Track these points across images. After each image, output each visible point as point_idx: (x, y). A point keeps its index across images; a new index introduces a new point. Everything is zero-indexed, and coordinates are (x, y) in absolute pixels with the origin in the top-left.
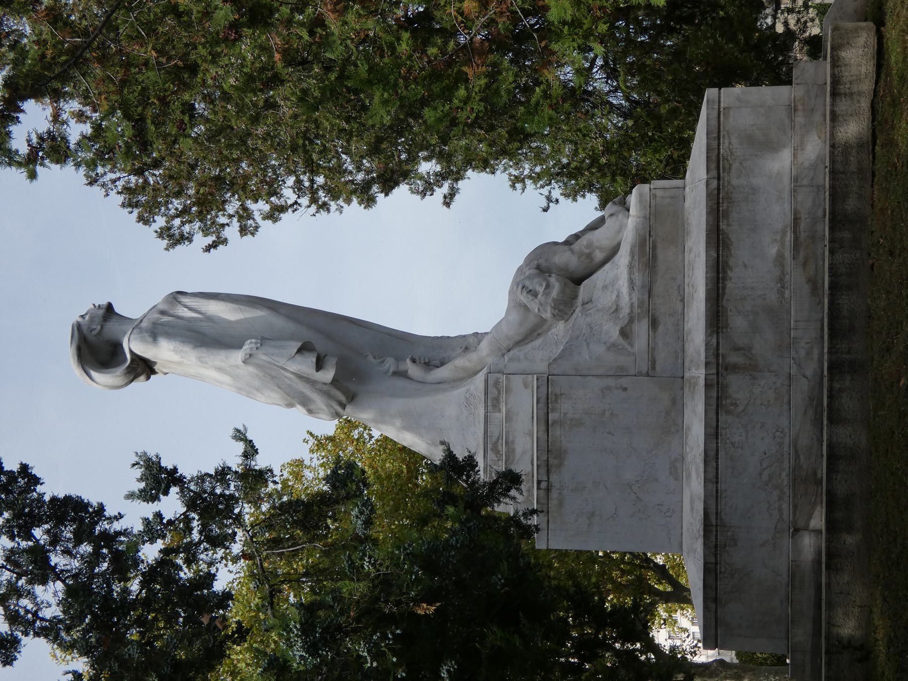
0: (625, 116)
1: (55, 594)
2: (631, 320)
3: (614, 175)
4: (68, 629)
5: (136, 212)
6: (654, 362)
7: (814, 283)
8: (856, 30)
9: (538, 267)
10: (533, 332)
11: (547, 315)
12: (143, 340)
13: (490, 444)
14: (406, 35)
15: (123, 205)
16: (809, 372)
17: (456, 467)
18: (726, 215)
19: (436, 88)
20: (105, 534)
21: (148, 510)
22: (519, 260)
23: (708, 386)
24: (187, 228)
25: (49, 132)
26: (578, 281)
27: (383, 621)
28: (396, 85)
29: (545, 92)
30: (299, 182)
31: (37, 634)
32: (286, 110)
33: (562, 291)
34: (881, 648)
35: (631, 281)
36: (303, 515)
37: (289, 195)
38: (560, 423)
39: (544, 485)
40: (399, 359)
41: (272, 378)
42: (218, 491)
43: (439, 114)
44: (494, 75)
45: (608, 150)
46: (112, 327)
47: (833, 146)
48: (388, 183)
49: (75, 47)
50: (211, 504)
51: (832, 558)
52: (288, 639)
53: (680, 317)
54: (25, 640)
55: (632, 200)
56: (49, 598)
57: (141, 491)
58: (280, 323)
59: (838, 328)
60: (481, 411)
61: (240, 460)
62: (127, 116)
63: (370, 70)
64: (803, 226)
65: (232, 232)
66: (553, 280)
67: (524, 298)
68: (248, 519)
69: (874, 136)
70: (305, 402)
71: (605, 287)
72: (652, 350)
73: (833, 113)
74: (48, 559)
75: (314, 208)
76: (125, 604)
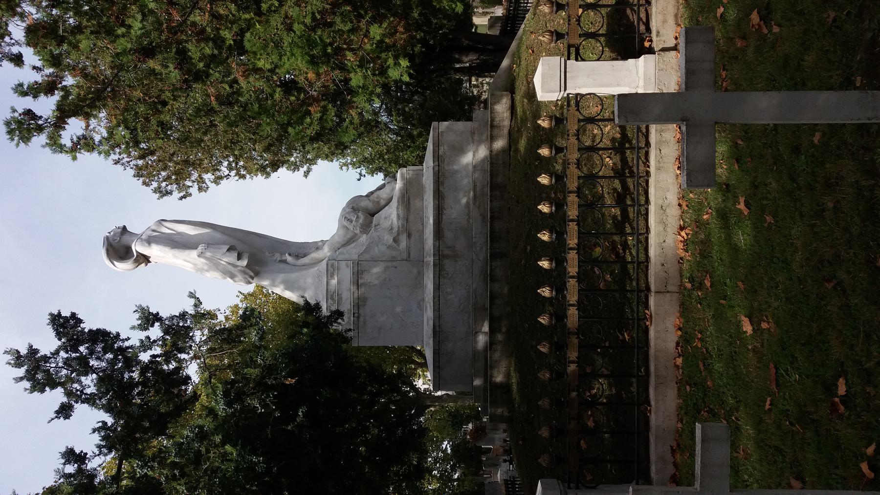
0: (397, 134)
1: (92, 381)
2: (398, 234)
3: (390, 163)
4: (100, 399)
5: (141, 179)
6: (409, 254)
7: (483, 216)
8: (502, 96)
9: (353, 208)
10: (351, 240)
11: (358, 231)
12: (143, 245)
13: (329, 295)
14: (278, 89)
15: (134, 176)
16: (481, 258)
17: (310, 309)
18: (443, 183)
19: (294, 118)
20: (120, 348)
21: (142, 335)
22: (344, 204)
23: (434, 265)
24: (169, 188)
25: (83, 135)
26: (373, 215)
27: (267, 388)
28: (274, 115)
29: (351, 121)
30: (230, 164)
31: (83, 402)
32: (221, 127)
33: (365, 220)
34: (515, 387)
35: (398, 215)
36: (226, 337)
37: (224, 170)
38: (364, 284)
39: (356, 315)
40: (283, 254)
41: (215, 265)
42: (181, 324)
43: (297, 131)
44: (324, 110)
45: (388, 152)
46: (126, 238)
47: (491, 151)
48: (275, 166)
49: (98, 90)
50: (177, 333)
51: (491, 344)
52: (216, 400)
53: (422, 232)
54: (76, 406)
55: (398, 175)
56: (89, 383)
57: (140, 325)
58: (218, 235)
59: (494, 237)
60: (325, 280)
61: (192, 308)
62: (127, 128)
63: (260, 107)
64: (478, 189)
65: (194, 190)
66: (360, 214)
67: (345, 223)
68: (197, 339)
69: (510, 147)
70: (232, 276)
71: (386, 218)
72: (408, 248)
73: (491, 135)
74: (89, 363)
75: (237, 178)
76: (132, 384)
